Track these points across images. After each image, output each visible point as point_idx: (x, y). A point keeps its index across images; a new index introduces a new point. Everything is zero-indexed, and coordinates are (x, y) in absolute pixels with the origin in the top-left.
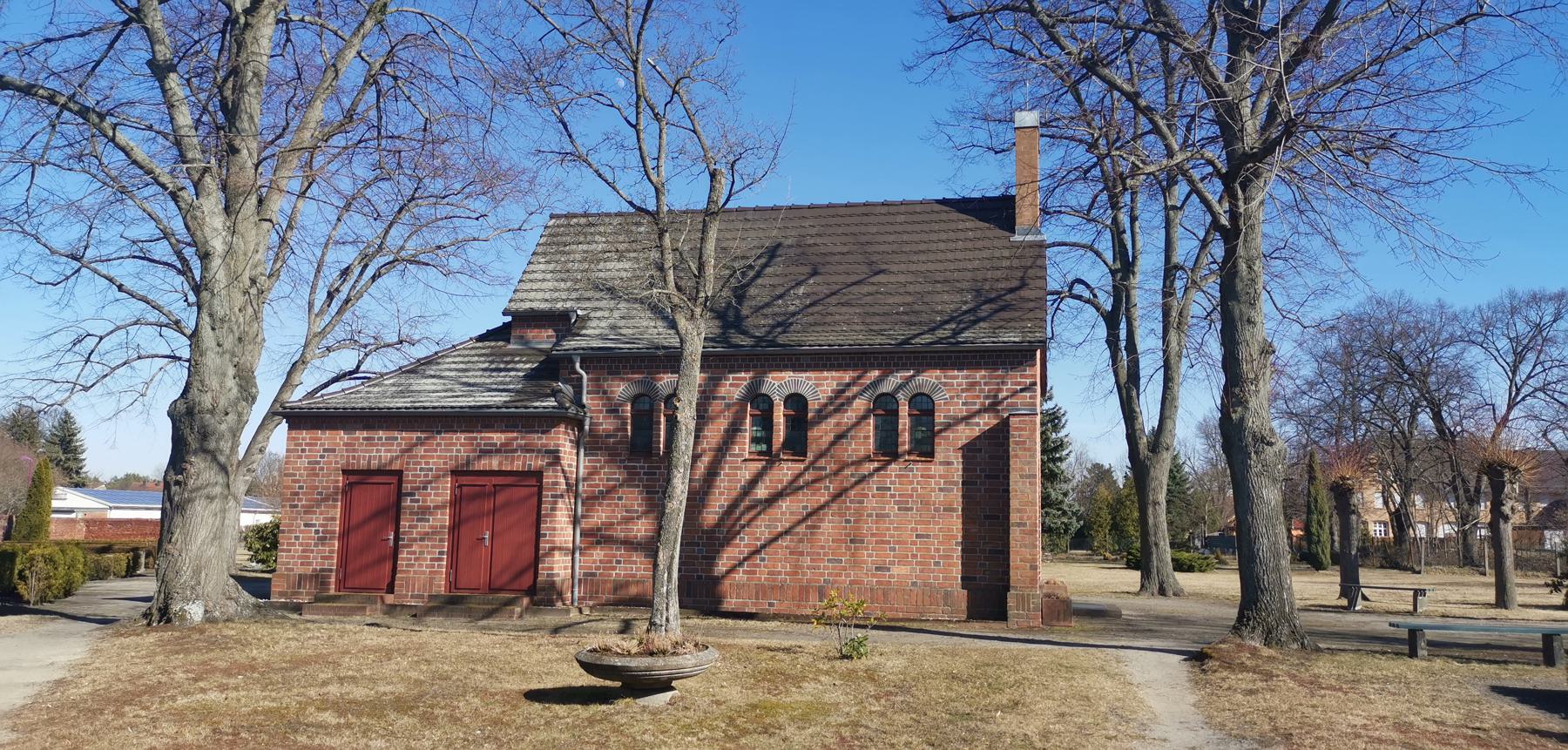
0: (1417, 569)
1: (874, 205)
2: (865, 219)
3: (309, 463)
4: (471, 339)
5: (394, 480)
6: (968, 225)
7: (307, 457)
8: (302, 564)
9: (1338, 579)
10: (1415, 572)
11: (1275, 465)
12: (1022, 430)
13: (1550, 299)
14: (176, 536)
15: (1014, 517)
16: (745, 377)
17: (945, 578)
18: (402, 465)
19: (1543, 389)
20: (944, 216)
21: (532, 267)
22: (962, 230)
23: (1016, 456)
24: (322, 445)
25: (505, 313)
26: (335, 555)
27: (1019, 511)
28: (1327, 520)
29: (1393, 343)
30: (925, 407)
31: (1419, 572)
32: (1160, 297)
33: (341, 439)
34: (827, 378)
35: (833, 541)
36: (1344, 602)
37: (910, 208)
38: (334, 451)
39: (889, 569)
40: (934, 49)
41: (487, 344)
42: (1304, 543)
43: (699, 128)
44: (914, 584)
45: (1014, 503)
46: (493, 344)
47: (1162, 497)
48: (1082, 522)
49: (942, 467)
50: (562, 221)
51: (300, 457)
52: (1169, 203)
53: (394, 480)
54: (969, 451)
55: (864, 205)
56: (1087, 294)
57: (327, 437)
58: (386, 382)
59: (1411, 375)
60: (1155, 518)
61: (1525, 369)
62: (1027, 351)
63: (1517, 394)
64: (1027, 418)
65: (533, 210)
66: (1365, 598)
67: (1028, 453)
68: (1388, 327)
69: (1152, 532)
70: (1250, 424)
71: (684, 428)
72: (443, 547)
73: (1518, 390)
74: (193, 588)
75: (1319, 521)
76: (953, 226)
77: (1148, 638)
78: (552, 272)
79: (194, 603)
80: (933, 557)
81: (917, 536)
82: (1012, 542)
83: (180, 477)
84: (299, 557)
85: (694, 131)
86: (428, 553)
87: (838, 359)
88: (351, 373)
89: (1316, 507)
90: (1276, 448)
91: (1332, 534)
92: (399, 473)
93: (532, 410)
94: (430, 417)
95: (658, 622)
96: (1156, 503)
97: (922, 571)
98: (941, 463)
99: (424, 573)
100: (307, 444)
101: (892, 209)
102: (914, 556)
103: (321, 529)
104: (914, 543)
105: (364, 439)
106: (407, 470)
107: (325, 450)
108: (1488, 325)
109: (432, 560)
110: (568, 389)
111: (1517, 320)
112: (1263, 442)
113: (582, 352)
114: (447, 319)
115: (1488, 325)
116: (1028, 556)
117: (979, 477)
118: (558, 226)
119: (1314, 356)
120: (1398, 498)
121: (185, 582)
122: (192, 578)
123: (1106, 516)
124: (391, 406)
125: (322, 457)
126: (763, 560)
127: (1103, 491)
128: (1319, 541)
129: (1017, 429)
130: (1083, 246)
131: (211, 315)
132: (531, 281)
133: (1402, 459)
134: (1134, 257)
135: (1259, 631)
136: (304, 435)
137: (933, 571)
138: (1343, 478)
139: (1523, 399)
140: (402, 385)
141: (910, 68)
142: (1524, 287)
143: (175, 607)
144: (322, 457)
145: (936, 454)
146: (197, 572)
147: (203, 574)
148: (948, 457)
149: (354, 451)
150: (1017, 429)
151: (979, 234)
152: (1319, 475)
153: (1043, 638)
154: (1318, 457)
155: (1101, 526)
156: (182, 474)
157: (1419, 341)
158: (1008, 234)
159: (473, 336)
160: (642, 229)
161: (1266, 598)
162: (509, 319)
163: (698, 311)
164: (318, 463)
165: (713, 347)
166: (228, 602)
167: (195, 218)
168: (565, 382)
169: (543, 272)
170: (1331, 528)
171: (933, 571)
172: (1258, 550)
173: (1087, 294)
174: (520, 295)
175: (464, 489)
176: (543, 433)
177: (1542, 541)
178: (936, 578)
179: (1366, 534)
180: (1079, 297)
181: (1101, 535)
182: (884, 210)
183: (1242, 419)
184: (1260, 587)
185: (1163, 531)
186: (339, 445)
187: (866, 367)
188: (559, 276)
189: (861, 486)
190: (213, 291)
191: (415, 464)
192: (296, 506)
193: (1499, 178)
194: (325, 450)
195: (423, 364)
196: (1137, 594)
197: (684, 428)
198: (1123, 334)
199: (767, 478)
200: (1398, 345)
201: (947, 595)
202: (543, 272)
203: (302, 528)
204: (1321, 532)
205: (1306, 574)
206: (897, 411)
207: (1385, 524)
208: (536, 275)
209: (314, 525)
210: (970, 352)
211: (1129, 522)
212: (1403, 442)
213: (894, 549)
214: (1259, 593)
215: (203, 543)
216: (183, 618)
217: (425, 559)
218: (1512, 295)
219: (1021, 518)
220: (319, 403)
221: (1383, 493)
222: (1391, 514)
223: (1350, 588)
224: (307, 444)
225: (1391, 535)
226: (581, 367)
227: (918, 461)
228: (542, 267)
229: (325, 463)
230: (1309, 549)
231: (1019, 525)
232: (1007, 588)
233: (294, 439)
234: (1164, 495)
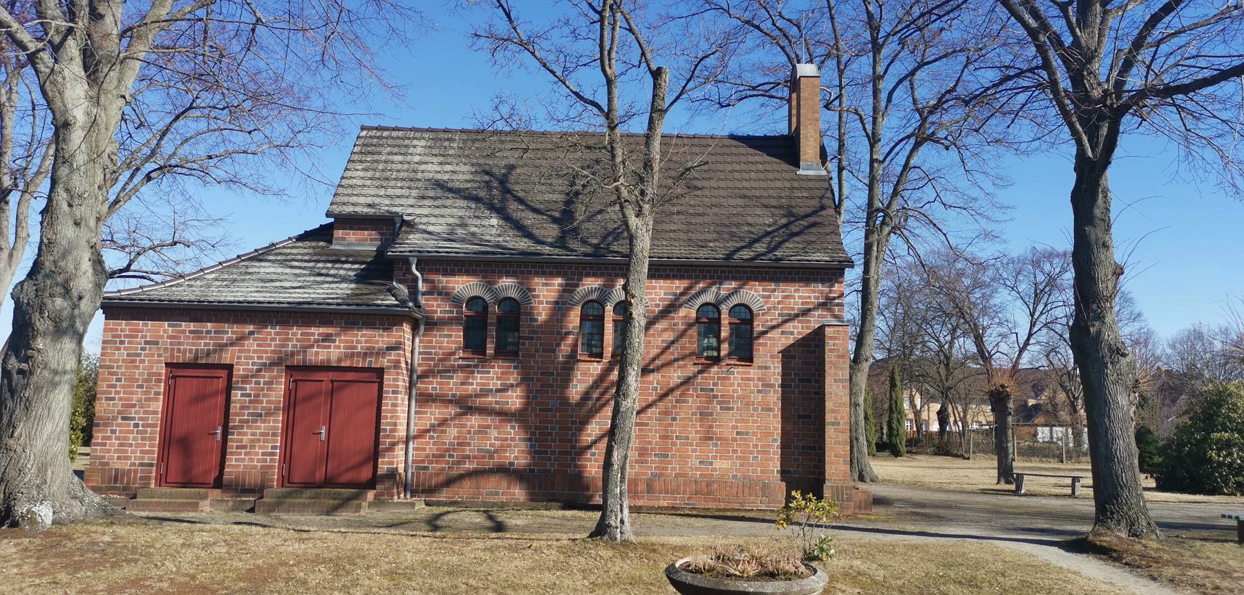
0: (966, 456)
3: (128, 355)
4: (290, 239)
5: (223, 374)
6: (757, 159)
7: (126, 349)
8: (119, 458)
9: (995, 464)
10: (965, 458)
11: (1128, 374)
12: (836, 338)
14: (19, 430)
15: (829, 417)
16: (420, 297)
17: (762, 472)
18: (232, 358)
19: (1045, 325)
20: (734, 150)
21: (349, 174)
24: (143, 337)
25: (328, 215)
26: (156, 449)
27: (833, 411)
30: (743, 316)
31: (968, 459)
33: (165, 331)
34: (654, 288)
38: (157, 343)
39: (711, 464)
40: (674, 13)
41: (308, 244)
43: (634, 26)
44: (734, 477)
45: (829, 405)
46: (314, 244)
49: (760, 371)
50: (373, 133)
51: (119, 349)
52: (875, 157)
53: (223, 374)
54: (787, 355)
57: (148, 328)
58: (207, 276)
62: (836, 269)
64: (840, 329)
65: (301, 129)
70: (1106, 337)
71: (637, 324)
72: (276, 441)
74: (38, 487)
75: (898, 419)
76: (744, 159)
77: (1040, 535)
78: (370, 179)
79: (41, 503)
81: (738, 433)
82: (827, 440)
83: (24, 366)
84: (116, 451)
85: (631, 30)
86: (260, 447)
87: (666, 270)
88: (121, 271)
89: (896, 408)
90: (1128, 359)
92: (229, 367)
93: (374, 308)
94: (264, 311)
95: (614, 524)
97: (742, 465)
98: (759, 368)
99: (255, 467)
100: (126, 336)
102: (735, 451)
103: (141, 423)
104: (735, 440)
105: (191, 332)
106: (238, 364)
107: (146, 343)
109: (263, 454)
110: (403, 290)
112: (1118, 353)
113: (417, 254)
114: (222, 224)
116: (842, 452)
117: (793, 380)
118: (371, 137)
121: (30, 481)
122: (38, 476)
124: (222, 299)
125: (142, 349)
126: (593, 454)
128: (898, 434)
131: (67, 190)
132: (351, 186)
135: (1123, 524)
136: (123, 325)
137: (752, 465)
138: (1003, 386)
140: (225, 280)
143: (21, 509)
144: (142, 349)
145: (755, 359)
146: (42, 469)
147: (49, 472)
149: (179, 344)
151: (768, 167)
153: (855, 526)
156: (26, 362)
158: (793, 168)
159: (292, 236)
160: (455, 145)
161: (1126, 493)
162: (332, 220)
163: (647, 207)
164: (139, 355)
165: (567, 255)
166: (73, 502)
167: (54, 83)
168: (400, 282)
169: (362, 178)
171: (752, 465)
172: (1116, 451)
174: (338, 199)
175: (335, 383)
176: (384, 329)
177: (1035, 435)
178: (755, 472)
183: (1099, 333)
184: (1119, 484)
186: (162, 337)
187: (698, 279)
188: (377, 183)
190: (72, 164)
191: (247, 358)
192: (113, 399)
194: (146, 343)
195: (243, 261)
197: (637, 324)
199: (591, 380)
201: (765, 487)
202: (362, 178)
203: (120, 421)
205: (889, 460)
208: (355, 181)
209: (134, 419)
210: (787, 268)
213: (717, 445)
214: (1119, 489)
215: (48, 439)
216: (33, 521)
217: (257, 454)
220: (139, 294)
224: (126, 336)
226: (417, 269)
227: (739, 365)
228: (361, 174)
229: (146, 355)
231: (833, 424)
232: (823, 481)
233: (112, 330)
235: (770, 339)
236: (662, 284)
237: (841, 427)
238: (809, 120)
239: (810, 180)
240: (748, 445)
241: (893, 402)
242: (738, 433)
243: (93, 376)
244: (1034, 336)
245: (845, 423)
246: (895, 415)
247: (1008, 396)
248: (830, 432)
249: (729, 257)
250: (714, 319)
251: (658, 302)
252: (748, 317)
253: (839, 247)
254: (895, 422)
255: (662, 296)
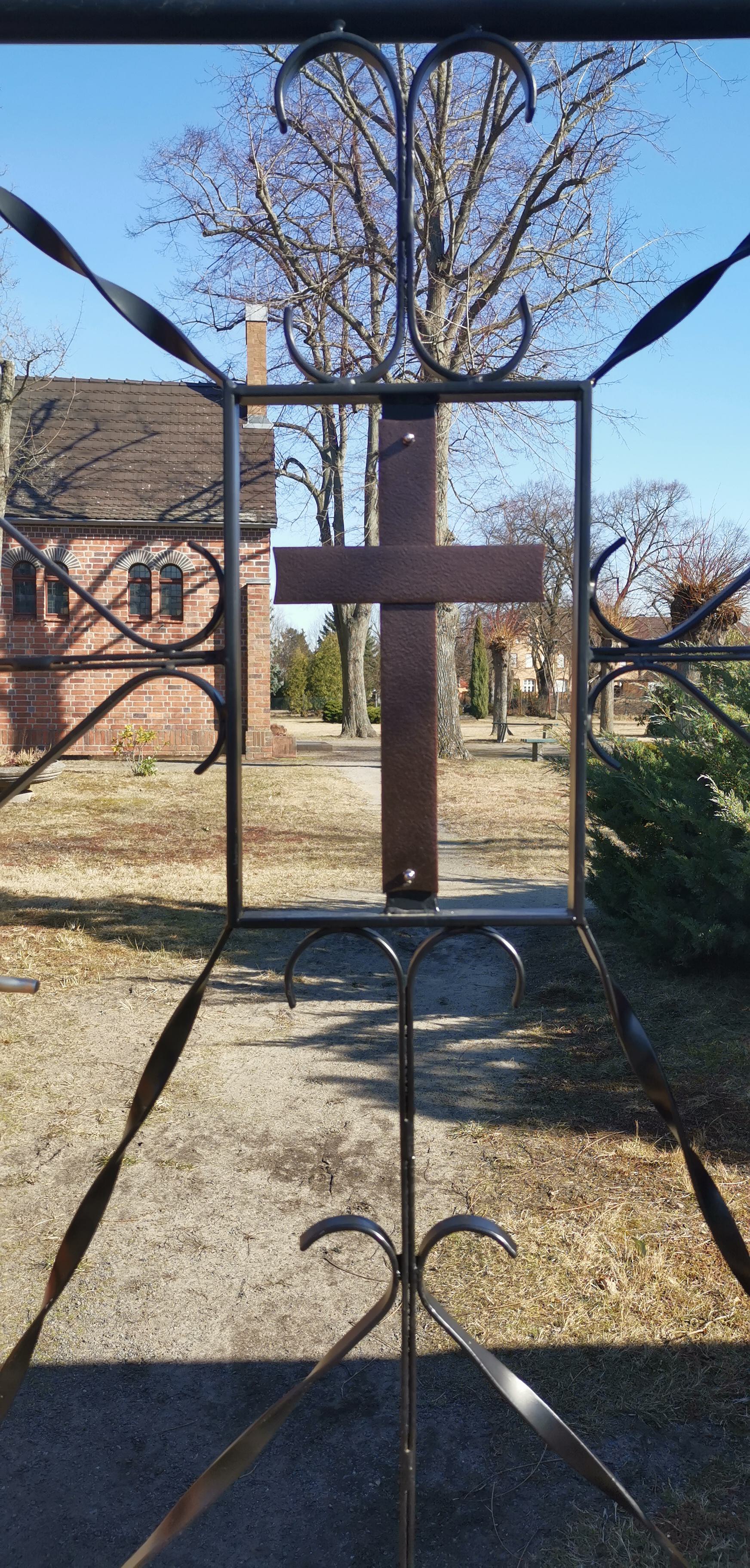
1: (117, 383)
2: (109, 397)
11: (451, 627)
13: (666, 489)
22: (200, 414)
23: (253, 619)
27: (255, 665)
28: (487, 676)
29: (546, 522)
30: (174, 576)
32: (362, 480)
34: (84, 548)
35: (96, 692)
36: (495, 737)
37: (151, 389)
40: (161, 217)
42: (468, 699)
47: (361, 656)
48: (282, 683)
49: (190, 629)
55: (107, 382)
56: (300, 474)
59: (559, 551)
60: (355, 673)
61: (643, 547)
63: (636, 569)
66: (510, 733)
67: (263, 617)
68: (543, 508)
69: (352, 685)
73: (637, 566)
75: (481, 678)
80: (183, 704)
81: (170, 687)
90: (452, 614)
91: (490, 689)
96: (356, 660)
98: (189, 625)
101: (135, 389)
104: (166, 693)
108: (618, 510)
111: (640, 506)
115: (618, 510)
119: (484, 531)
120: (543, 658)
123: (302, 676)
127: (300, 655)
128: (480, 694)
129: (253, 597)
130: (298, 428)
133: (547, 623)
134: (342, 442)
138: (499, 639)
139: (640, 573)
141: (134, 234)
142: (648, 477)
145: (185, 617)
148: (195, 619)
150: (253, 597)
152: (482, 637)
154: (483, 622)
155: (297, 687)
157: (566, 521)
170: (490, 684)
173: (300, 474)
179: (517, 690)
180: (292, 476)
181: (297, 695)
182: (126, 389)
185: (361, 685)
189: (117, 645)
193: (606, 419)
196: (340, 737)
198: (331, 512)
200: (550, 525)
204: (482, 687)
206: (150, 579)
207: (533, 681)
210: (213, 528)
211: (323, 683)
212: (549, 610)
218: (638, 485)
219: (257, 671)
221: (532, 654)
222: (537, 671)
223: (501, 728)
225: (537, 690)
230: (472, 702)
231: (255, 676)
234: (363, 654)
235: (199, 597)
236: (92, 545)
237: (262, 679)
238: (256, 369)
239: (256, 434)
240: (180, 699)
241: (476, 659)
242: (170, 687)
243: (596, 989)
244: (636, 580)
245: (266, 676)
246: (478, 674)
247: (504, 648)
248: (252, 683)
249: (161, 518)
250: (145, 579)
251: (89, 563)
252: (179, 576)
253: (272, 505)
254: (477, 681)
255: (93, 557)
